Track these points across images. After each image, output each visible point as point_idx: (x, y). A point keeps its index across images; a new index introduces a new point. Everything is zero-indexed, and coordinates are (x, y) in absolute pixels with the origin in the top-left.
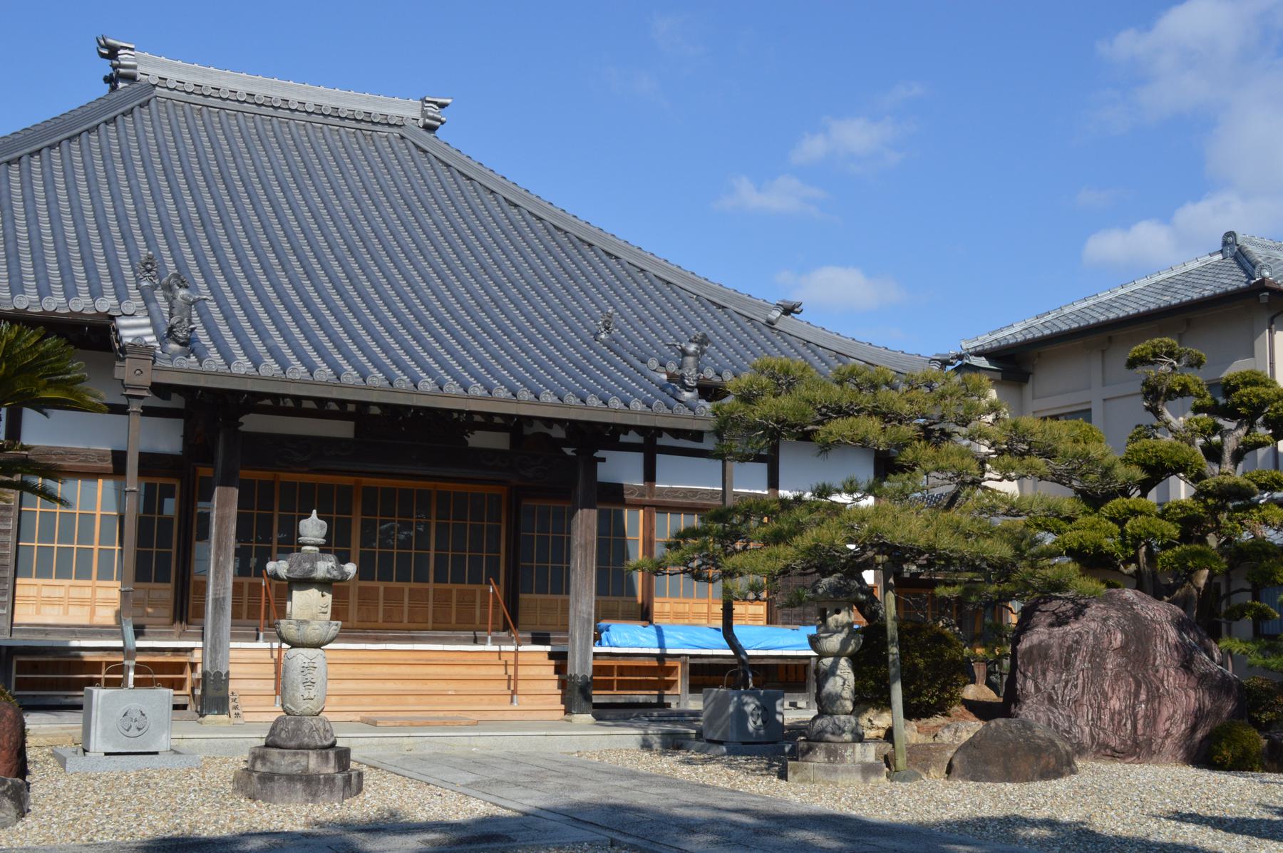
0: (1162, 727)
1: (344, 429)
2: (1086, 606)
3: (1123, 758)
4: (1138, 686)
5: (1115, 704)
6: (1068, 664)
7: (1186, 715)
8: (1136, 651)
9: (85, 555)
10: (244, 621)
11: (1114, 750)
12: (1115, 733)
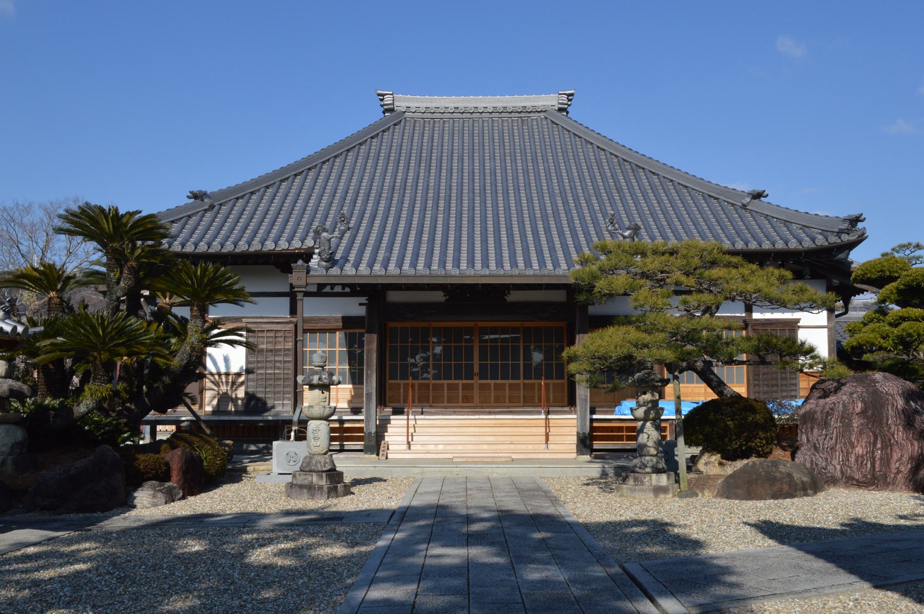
0: (894, 466)
1: (439, 297)
2: (844, 385)
3: (866, 487)
4: (876, 439)
5: (859, 450)
6: (826, 424)
7: (911, 458)
8: (873, 414)
9: (516, 367)
10: (416, 404)
11: (857, 481)
12: (858, 470)
